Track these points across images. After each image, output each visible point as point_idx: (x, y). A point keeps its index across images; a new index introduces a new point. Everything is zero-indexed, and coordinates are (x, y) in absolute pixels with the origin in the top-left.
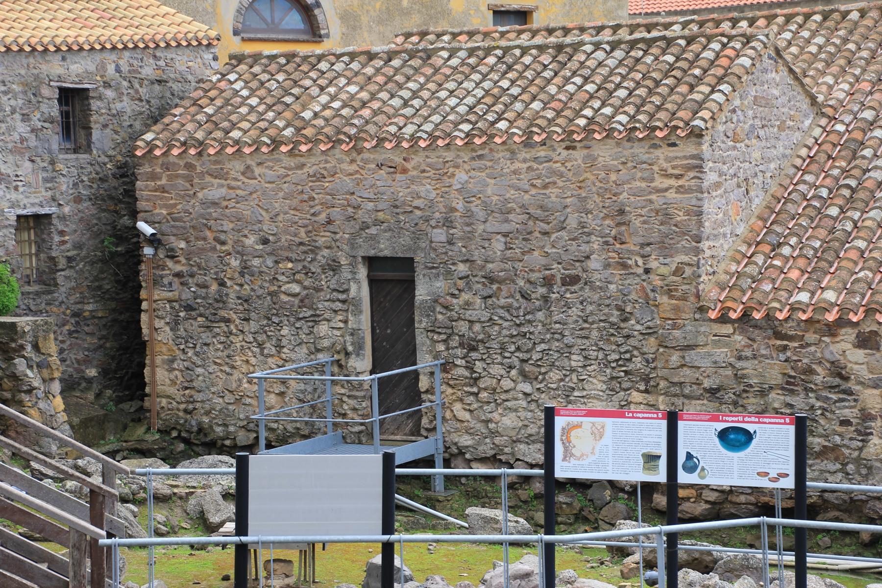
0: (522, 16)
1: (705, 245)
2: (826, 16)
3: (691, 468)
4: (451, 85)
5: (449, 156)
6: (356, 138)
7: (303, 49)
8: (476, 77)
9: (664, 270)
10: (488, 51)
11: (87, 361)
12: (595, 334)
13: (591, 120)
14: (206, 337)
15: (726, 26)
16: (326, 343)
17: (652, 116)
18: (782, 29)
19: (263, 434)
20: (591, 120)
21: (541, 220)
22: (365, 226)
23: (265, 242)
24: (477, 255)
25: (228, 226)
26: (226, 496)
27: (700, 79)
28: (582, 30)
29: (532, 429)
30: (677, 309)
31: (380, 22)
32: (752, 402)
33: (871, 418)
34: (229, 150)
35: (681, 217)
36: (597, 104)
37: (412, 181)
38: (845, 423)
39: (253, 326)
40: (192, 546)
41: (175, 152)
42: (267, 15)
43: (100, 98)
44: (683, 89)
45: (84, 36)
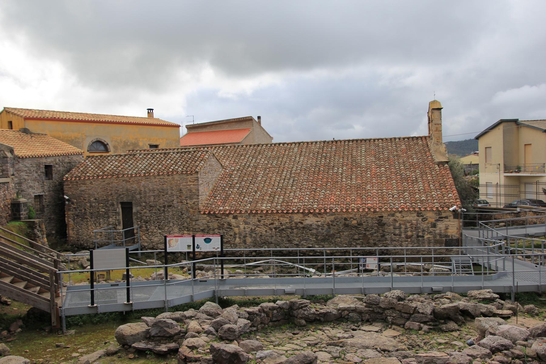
0: (156, 146)
1: (200, 197)
2: (223, 147)
3: (198, 248)
4: (140, 162)
5: (140, 178)
6: (118, 175)
7: (104, 154)
8: (146, 160)
9: (191, 203)
10: (148, 154)
11: (52, 230)
12: (175, 218)
13: (173, 170)
14: (81, 222)
15: (202, 149)
16: (111, 223)
17: (187, 168)
18: (214, 150)
19: (96, 245)
20: (173, 170)
21: (162, 192)
22: (120, 195)
23: (96, 199)
24: (147, 201)
25: (87, 196)
26: (88, 260)
27: (197, 160)
28: (170, 149)
29: (161, 241)
30: (194, 212)
31: (123, 148)
32: (211, 232)
33: (236, 234)
34: (87, 178)
35: (194, 191)
36: (174, 166)
37: (131, 184)
38: (231, 236)
39: (93, 219)
40: (80, 272)
41: (73, 179)
42: (95, 147)
43: (55, 167)
44: (193, 162)
45: (51, 153)
